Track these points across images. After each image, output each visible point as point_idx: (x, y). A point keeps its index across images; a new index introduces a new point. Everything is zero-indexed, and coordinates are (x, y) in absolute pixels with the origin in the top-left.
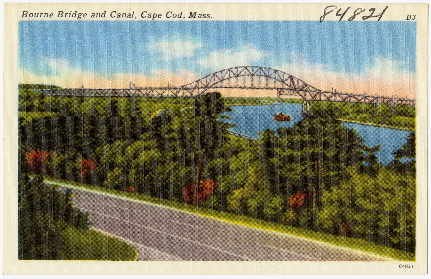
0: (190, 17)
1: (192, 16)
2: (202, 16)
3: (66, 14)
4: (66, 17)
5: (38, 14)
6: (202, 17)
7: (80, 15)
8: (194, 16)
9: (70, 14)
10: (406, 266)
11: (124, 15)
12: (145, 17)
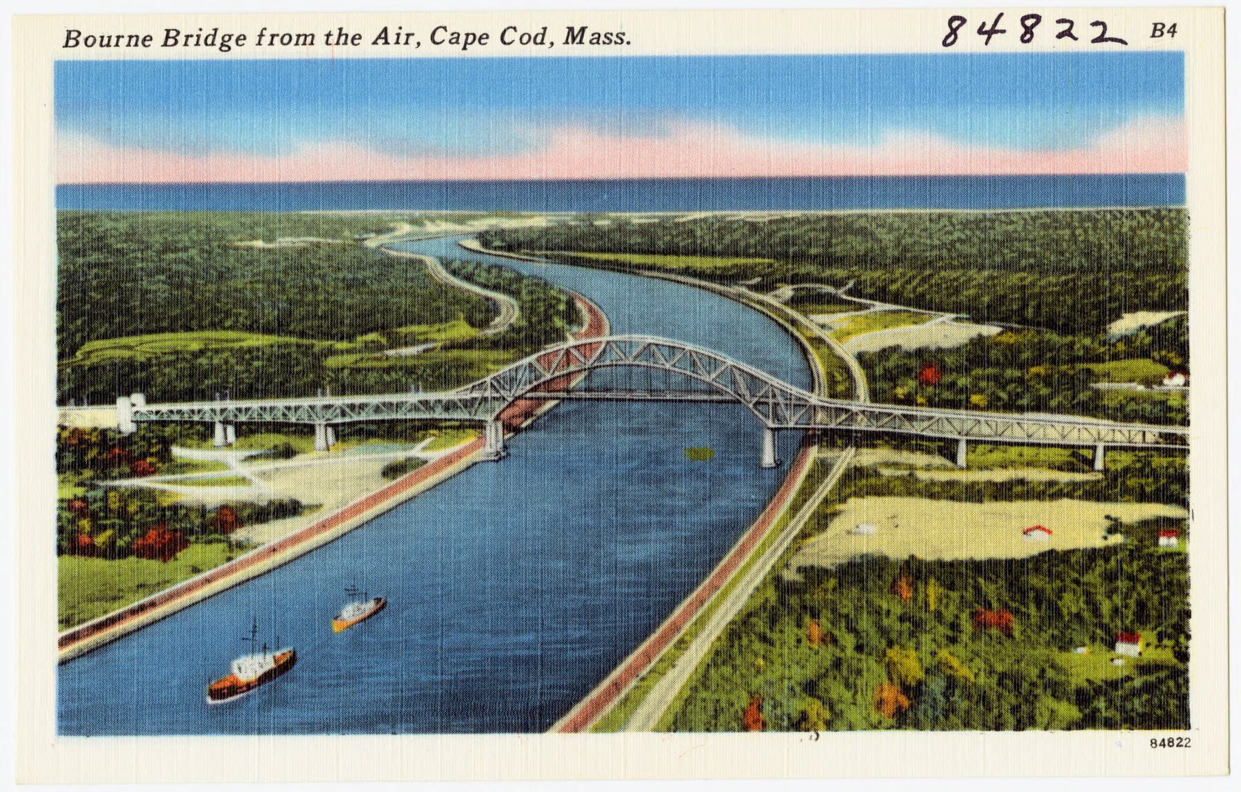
0: (567, 42)
1: (574, 39)
2: (602, 38)
3: (187, 37)
4: (186, 44)
5: (110, 38)
6: (601, 42)
7: (226, 38)
8: (578, 40)
9: (198, 36)
10: (1171, 741)
11: (302, 39)
12: (441, 43)
